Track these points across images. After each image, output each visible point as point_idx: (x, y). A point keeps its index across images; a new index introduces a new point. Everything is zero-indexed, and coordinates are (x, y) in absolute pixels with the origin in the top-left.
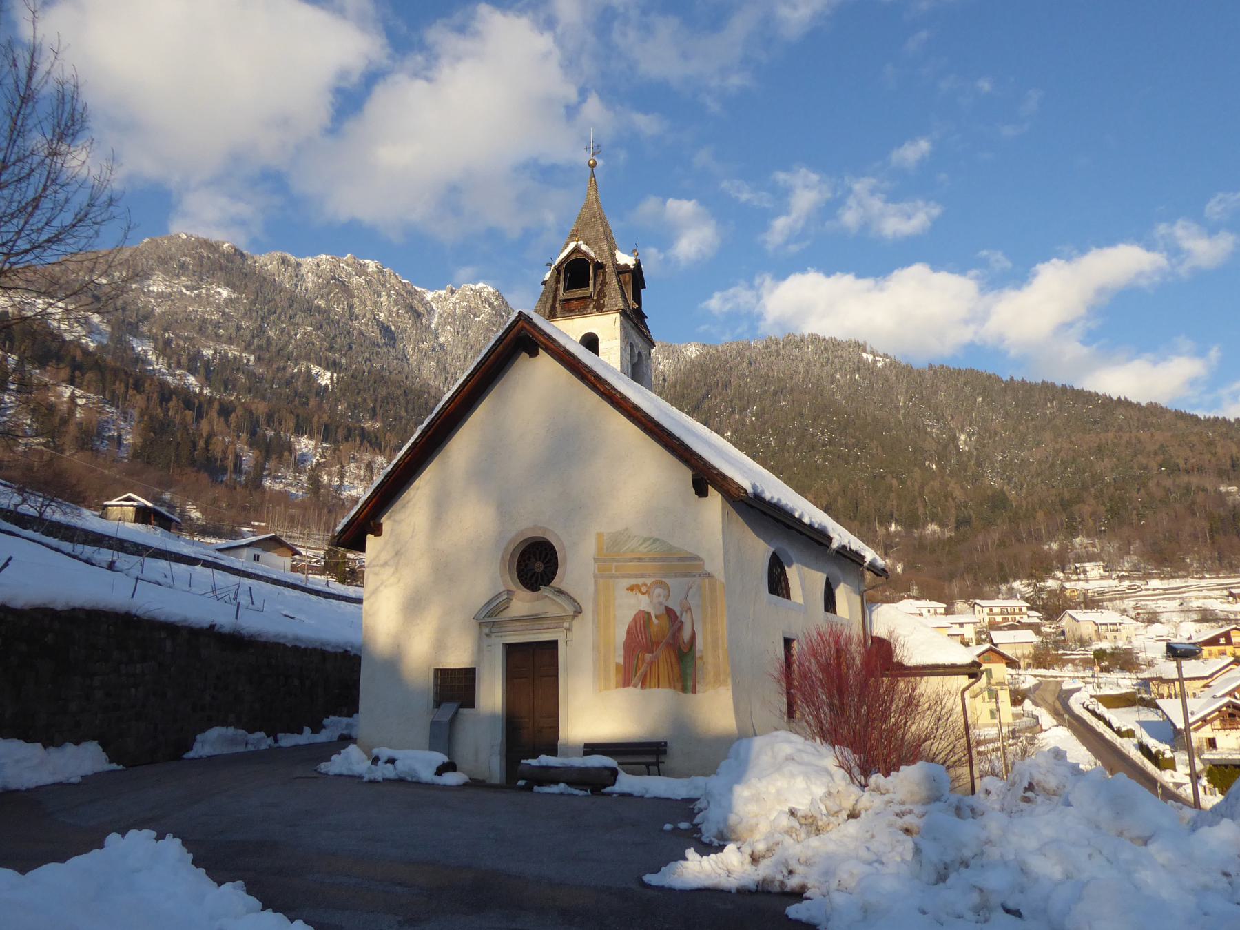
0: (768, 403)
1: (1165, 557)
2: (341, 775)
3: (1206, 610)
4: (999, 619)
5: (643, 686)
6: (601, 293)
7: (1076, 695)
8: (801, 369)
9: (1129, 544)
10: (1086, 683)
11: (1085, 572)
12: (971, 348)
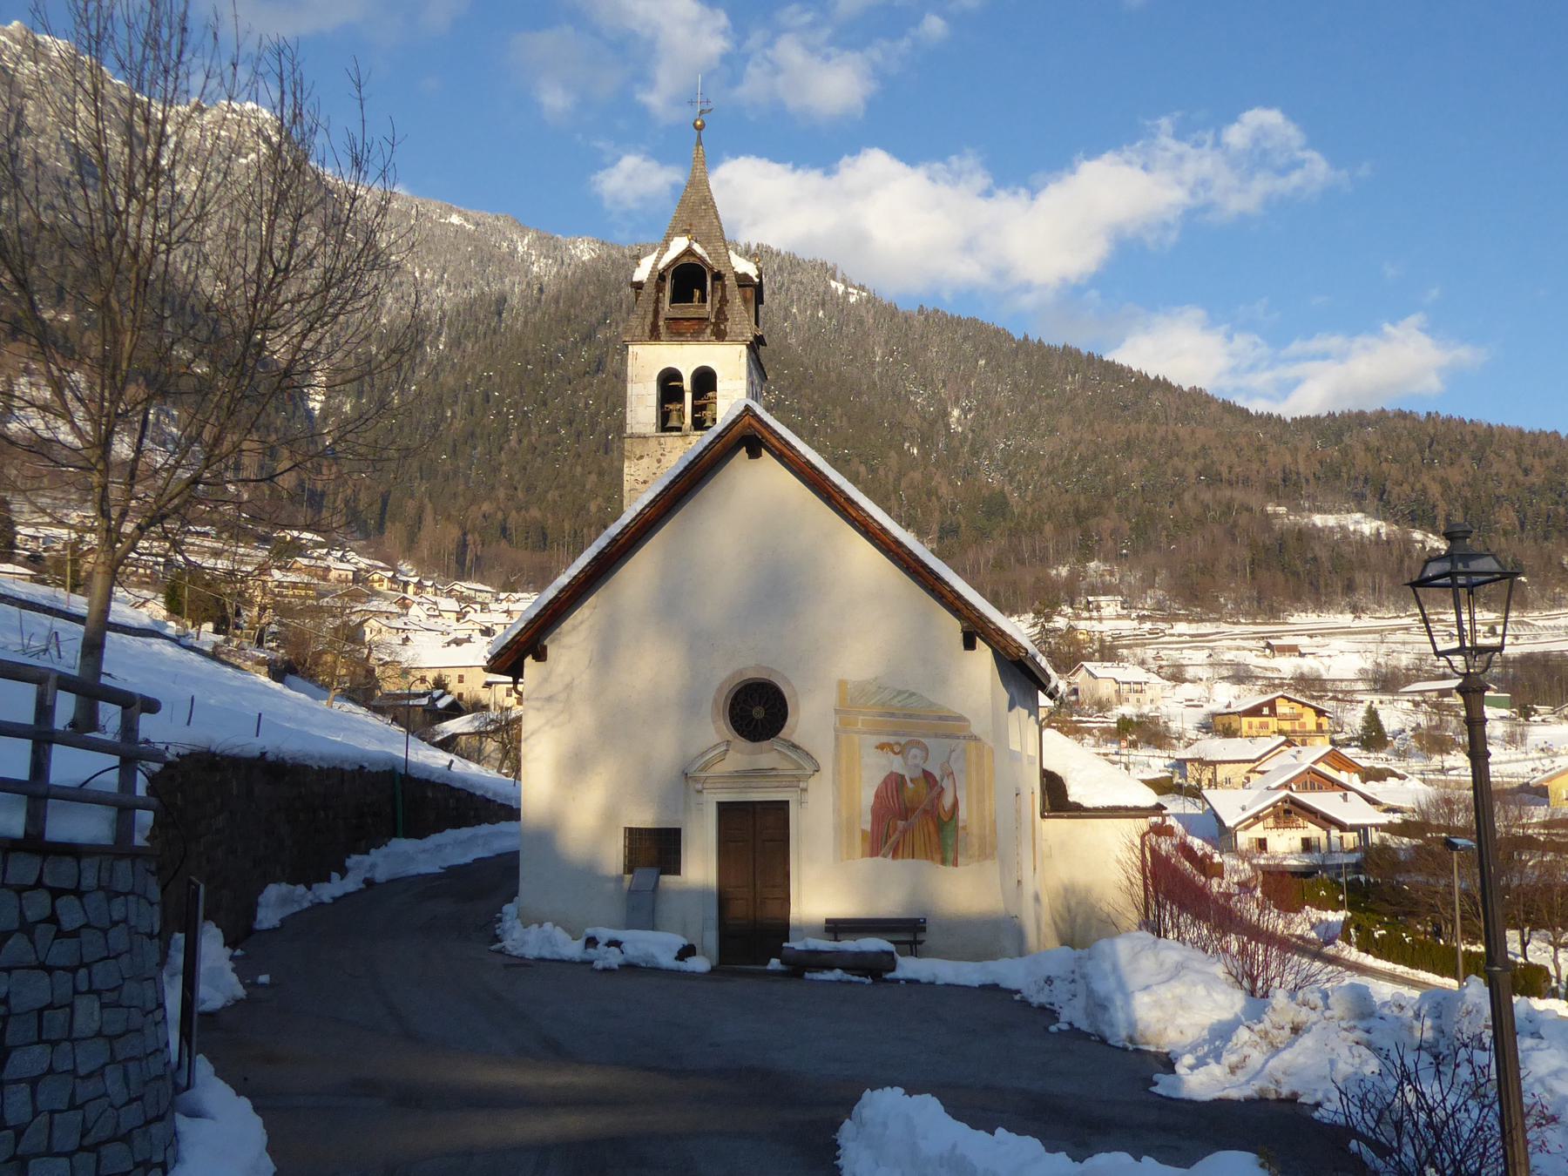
1: (1194, 593)
2: (542, 960)
3: (1238, 664)
5: (894, 856)
6: (721, 315)
9: (1155, 573)
11: (1098, 608)
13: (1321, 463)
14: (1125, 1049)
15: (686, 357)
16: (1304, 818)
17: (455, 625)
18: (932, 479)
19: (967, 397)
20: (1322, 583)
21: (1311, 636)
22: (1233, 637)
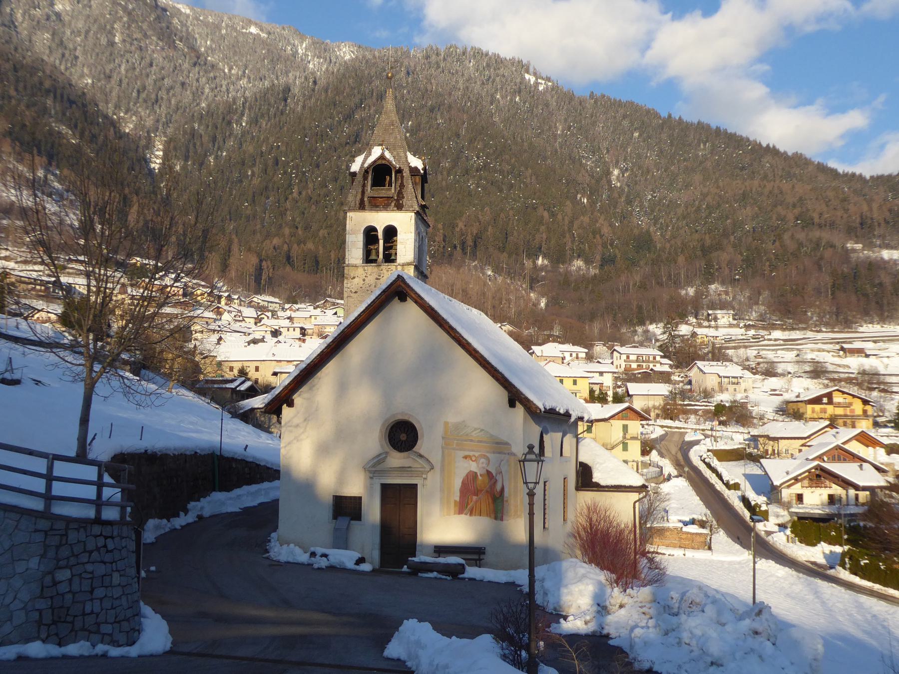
0: (424, 119)
1: (788, 310)
2: (288, 563)
4: (634, 366)
5: (471, 515)
6: (400, 195)
7: (696, 448)
8: (461, 85)
9: (760, 294)
10: (706, 436)
11: (716, 319)
12: (636, 76)
13: (890, 211)
14: (552, 613)
15: (380, 220)
16: (830, 481)
17: (254, 327)
18: (597, 221)
19: (625, 160)
20: (885, 302)
21: (875, 342)
22: (815, 341)
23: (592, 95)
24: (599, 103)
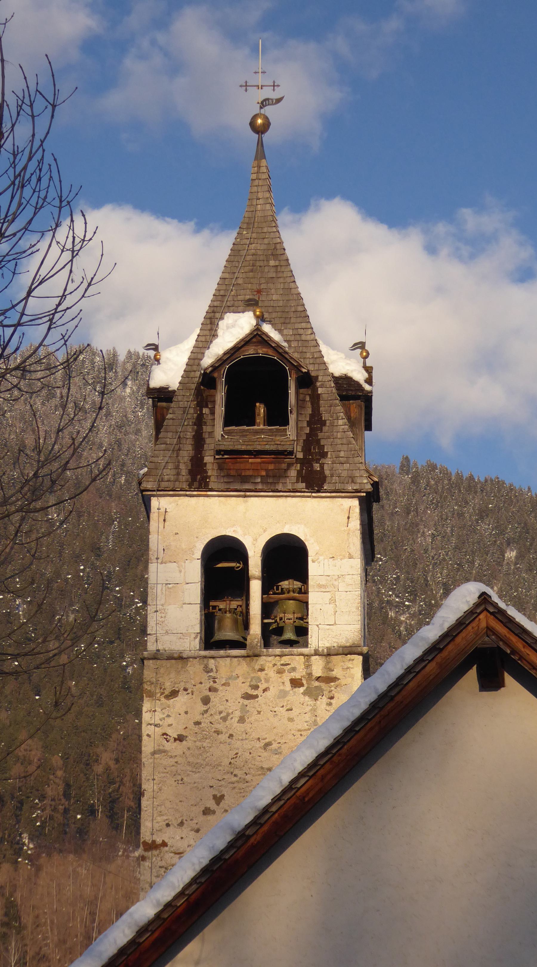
6: (313, 447)
15: (253, 520)
23: (406, 465)
24: (423, 483)
